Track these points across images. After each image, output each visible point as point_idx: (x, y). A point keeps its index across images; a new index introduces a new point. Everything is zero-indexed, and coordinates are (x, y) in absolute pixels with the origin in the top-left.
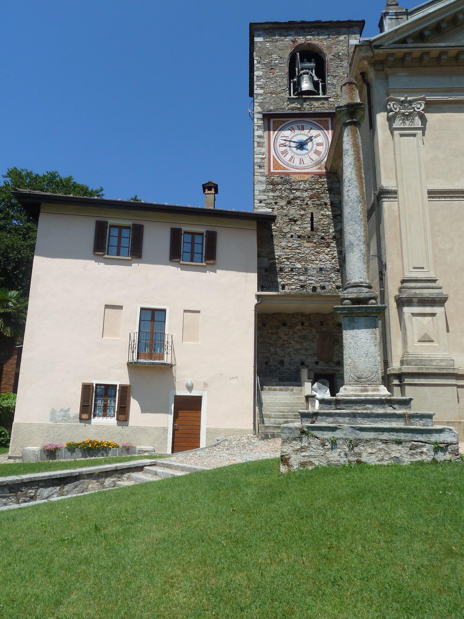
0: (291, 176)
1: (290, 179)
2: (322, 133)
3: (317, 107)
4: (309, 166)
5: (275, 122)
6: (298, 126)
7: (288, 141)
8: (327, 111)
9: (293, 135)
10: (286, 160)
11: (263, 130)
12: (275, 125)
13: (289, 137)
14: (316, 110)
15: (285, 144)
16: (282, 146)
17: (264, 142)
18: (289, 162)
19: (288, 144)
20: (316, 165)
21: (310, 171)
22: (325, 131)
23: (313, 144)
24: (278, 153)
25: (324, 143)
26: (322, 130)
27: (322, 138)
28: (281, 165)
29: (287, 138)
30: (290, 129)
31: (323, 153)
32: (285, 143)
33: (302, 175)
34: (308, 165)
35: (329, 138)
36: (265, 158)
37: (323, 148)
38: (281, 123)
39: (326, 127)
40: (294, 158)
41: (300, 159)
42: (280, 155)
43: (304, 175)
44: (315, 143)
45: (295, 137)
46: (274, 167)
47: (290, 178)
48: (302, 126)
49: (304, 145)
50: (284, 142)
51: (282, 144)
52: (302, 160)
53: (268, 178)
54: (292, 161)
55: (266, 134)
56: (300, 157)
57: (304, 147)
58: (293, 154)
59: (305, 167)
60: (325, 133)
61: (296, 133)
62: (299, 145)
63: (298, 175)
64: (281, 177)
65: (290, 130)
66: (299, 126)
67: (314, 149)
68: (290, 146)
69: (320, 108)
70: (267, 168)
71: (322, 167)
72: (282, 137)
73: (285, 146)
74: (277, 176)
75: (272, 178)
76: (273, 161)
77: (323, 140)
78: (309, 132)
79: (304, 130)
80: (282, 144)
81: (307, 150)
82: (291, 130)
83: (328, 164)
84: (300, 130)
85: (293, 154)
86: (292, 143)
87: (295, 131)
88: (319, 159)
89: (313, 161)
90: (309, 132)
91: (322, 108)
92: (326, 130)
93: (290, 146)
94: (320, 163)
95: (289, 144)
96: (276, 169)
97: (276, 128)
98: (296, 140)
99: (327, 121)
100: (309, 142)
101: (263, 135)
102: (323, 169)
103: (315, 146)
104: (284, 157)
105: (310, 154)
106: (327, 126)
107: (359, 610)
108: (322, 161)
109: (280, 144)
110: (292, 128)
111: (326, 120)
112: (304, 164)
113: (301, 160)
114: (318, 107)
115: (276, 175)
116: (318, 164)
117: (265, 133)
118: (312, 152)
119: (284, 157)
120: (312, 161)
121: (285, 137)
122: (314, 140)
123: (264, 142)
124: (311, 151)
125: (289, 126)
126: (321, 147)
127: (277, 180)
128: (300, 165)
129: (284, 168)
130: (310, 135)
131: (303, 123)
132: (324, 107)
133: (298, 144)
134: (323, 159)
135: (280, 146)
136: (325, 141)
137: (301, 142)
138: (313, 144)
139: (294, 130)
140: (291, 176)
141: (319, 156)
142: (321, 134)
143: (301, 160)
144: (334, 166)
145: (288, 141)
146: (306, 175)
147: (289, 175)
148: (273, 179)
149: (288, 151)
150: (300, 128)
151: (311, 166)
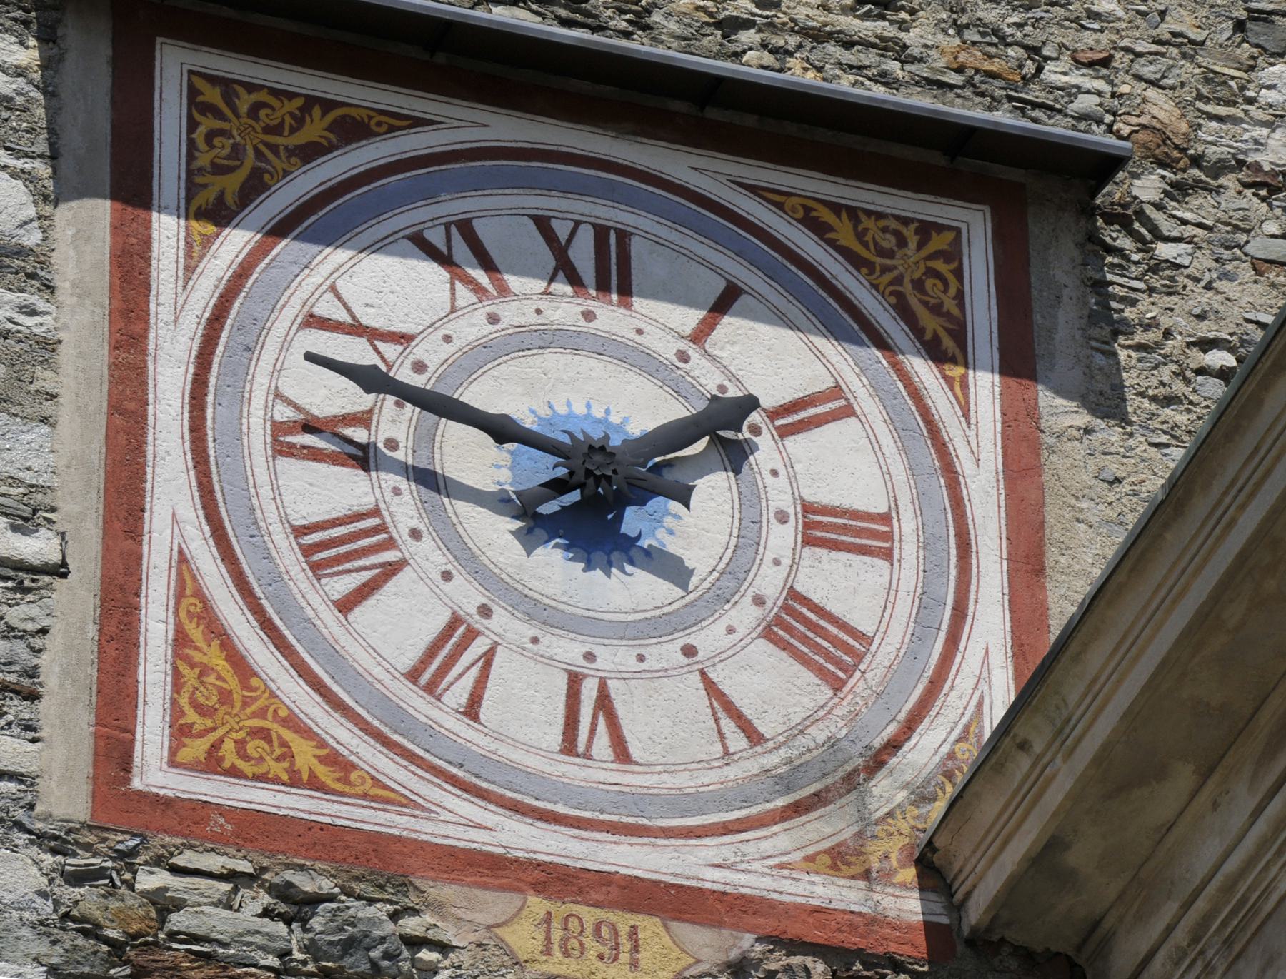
0: (437, 907)
1: (414, 943)
2: (876, 390)
3: (806, 32)
4: (695, 801)
5: (212, 95)
6: (542, 224)
7: (407, 394)
8: (923, 101)
9: (471, 328)
10: (364, 660)
11: (42, 169)
12: (223, 147)
13: (419, 351)
14: (795, 63)
15: (359, 435)
16: (315, 455)
17: (48, 346)
18: (414, 701)
19: (400, 434)
20: (798, 809)
21: (713, 879)
22: (923, 370)
23: (750, 501)
24: (256, 532)
25: (907, 525)
26: (881, 343)
27: (875, 444)
28: (293, 722)
29: (390, 350)
30: (436, 237)
31: (886, 651)
32: (363, 419)
33: (589, 915)
34: (683, 781)
35: (964, 463)
36: (60, 570)
37: (891, 589)
38: (315, 129)
39: (930, 323)
40: (478, 647)
41: (575, 681)
42: (276, 577)
43: (624, 921)
44: (779, 495)
45: (511, 368)
46: (180, 732)
47: (411, 925)
48: (601, 233)
49: (640, 492)
50: (348, 397)
51: (309, 427)
52: (604, 702)
53: (78, 878)
54: (458, 694)
55: (82, 237)
56: (570, 650)
57: (633, 520)
58: (466, 594)
59: (644, 799)
60: (916, 395)
61: (514, 314)
62: (557, 487)
63: (537, 905)
64: (284, 892)
65: (432, 253)
66: (562, 229)
67: (769, 582)
68: (427, 479)
69: (848, 57)
70: (84, 720)
71: (875, 850)
72: (314, 322)
73: (363, 458)
74: (214, 862)
75: (150, 880)
76: (181, 640)
77: (887, 474)
78: (700, 336)
79: (626, 291)
80: (309, 427)
81: (674, 570)
82: (445, 260)
83: (988, 808)
84: (575, 280)
85: (466, 594)
86: (455, 434)
87: (514, 282)
88: (835, 727)
89: (754, 737)
90: (700, 336)
91: (870, 57)
92: (937, 354)
93: (427, 479)
94: (852, 782)
95: (426, 439)
96: (212, 764)
97: (232, 183)
98: (523, 412)
99: (939, 242)
100: (701, 466)
101: (32, 238)
102: (887, 876)
103: (782, 538)
104: (346, 605)
105: (709, 639)
106: (936, 310)
107: (1222, 251)
108: (878, 761)
109: (284, 413)
110: (466, 228)
111: (926, 229)
112: (622, 753)
113: (589, 692)
114: (818, 36)
115: (217, 843)
116: (817, 801)
117: (64, 214)
118: (745, 615)
119: (346, 605)
120: (737, 741)
121: (356, 329)
122: (766, 452)
123: (48, 346)
124: (723, 597)
125: (428, 195)
126: (870, 572)
127: (214, 921)
128: (571, 771)
129: (335, 760)
130: (709, 380)
131: (631, 201)
132: (901, 53)
133: (545, 467)
134: (894, 746)
135: (282, 450)
136: (921, 500)
137: (599, 449)
138: (750, 501)
139: (488, 265)
140: (437, 907)
141: (837, 685)
142: (866, 402)
143: (589, 692)
144: (1078, 857)
145: (407, 394)
146: (649, 926)
147: (404, 886)
148: (164, 904)
149: (401, 531)
150: (583, 254)
151: (722, 799)
